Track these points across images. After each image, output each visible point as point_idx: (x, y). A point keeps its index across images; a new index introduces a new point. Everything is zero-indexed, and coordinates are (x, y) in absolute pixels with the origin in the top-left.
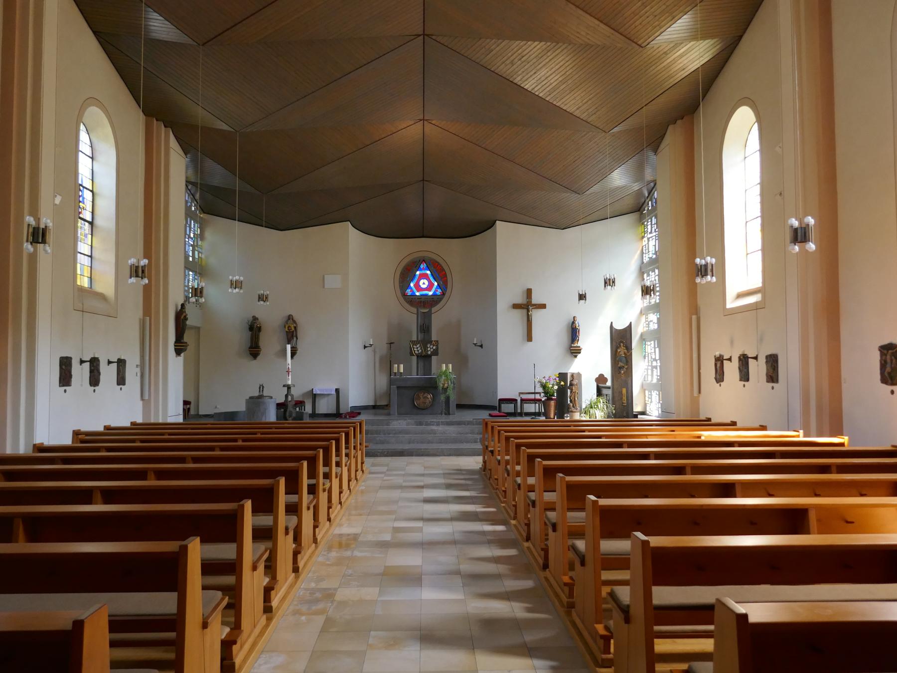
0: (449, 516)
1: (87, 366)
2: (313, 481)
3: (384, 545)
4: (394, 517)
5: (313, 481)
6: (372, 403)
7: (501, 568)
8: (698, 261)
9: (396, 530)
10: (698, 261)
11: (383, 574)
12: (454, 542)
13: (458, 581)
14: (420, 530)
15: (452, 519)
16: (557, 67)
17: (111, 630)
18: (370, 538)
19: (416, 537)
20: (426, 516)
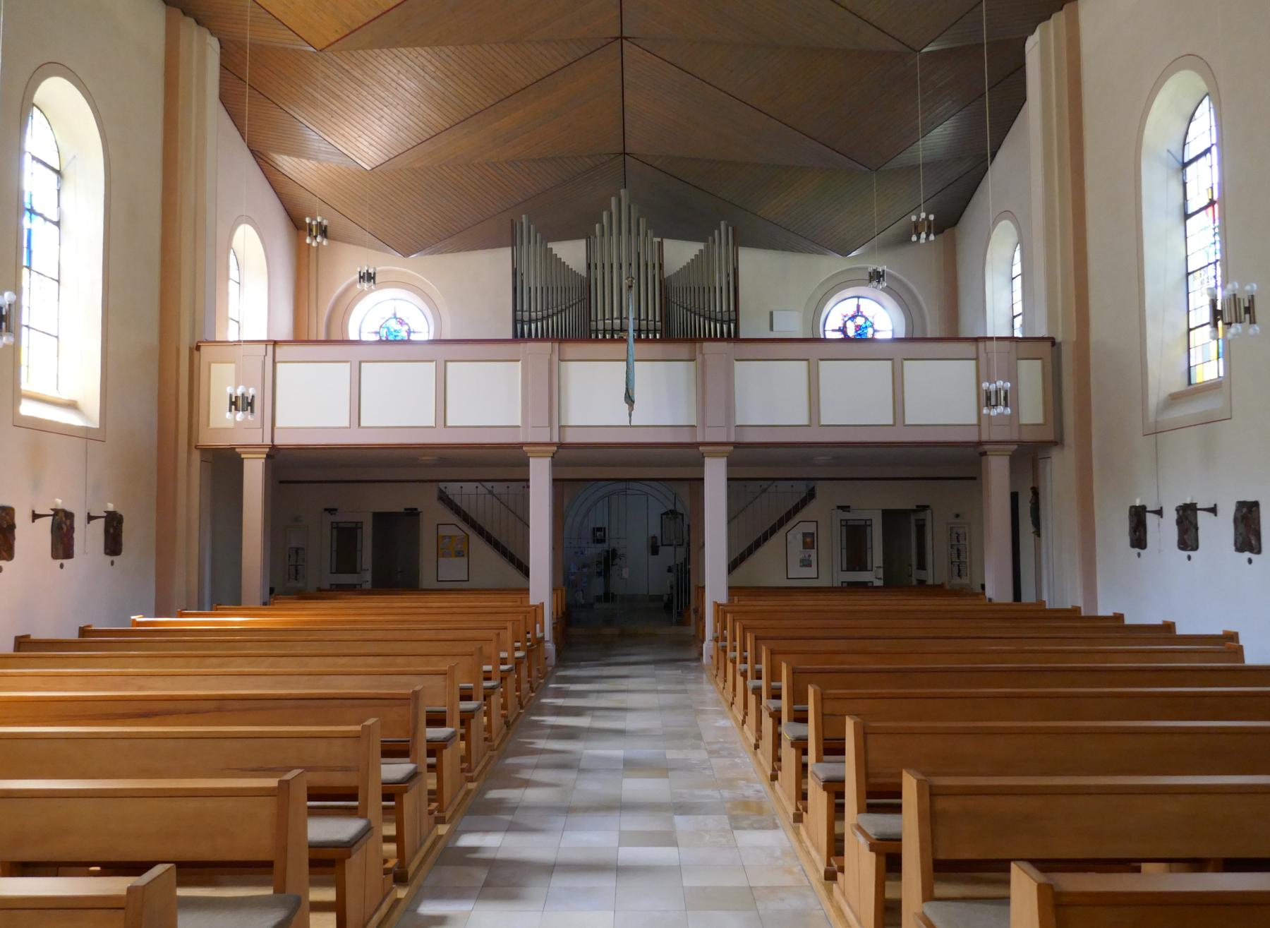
0: (559, 882)
1: (99, 525)
2: (758, 666)
3: (683, 808)
4: (689, 881)
5: (758, 666)
6: (291, 338)
7: (526, 775)
8: (1208, 369)
9: (669, 839)
10: (1208, 369)
11: (668, 770)
12: (569, 810)
13: (583, 764)
14: (627, 839)
15: (549, 869)
16: (431, 635)
17: (1008, 898)
18: (711, 821)
19: (634, 823)
20: (606, 882)
